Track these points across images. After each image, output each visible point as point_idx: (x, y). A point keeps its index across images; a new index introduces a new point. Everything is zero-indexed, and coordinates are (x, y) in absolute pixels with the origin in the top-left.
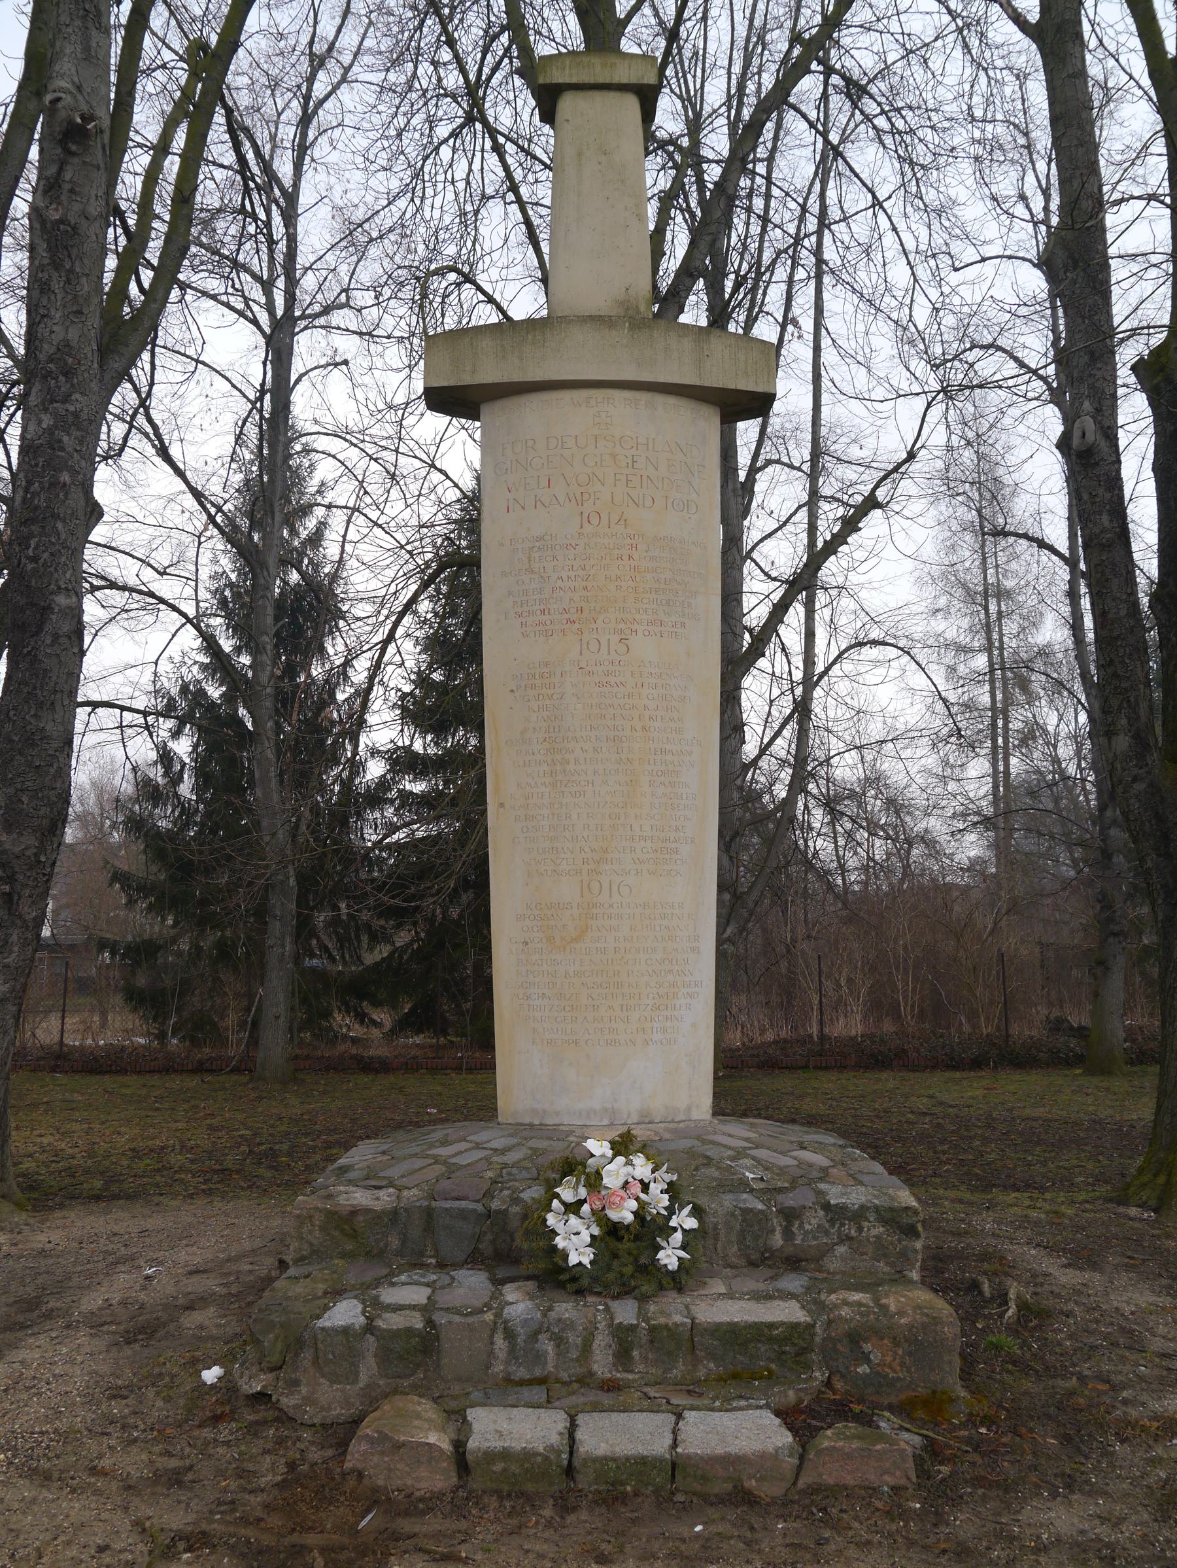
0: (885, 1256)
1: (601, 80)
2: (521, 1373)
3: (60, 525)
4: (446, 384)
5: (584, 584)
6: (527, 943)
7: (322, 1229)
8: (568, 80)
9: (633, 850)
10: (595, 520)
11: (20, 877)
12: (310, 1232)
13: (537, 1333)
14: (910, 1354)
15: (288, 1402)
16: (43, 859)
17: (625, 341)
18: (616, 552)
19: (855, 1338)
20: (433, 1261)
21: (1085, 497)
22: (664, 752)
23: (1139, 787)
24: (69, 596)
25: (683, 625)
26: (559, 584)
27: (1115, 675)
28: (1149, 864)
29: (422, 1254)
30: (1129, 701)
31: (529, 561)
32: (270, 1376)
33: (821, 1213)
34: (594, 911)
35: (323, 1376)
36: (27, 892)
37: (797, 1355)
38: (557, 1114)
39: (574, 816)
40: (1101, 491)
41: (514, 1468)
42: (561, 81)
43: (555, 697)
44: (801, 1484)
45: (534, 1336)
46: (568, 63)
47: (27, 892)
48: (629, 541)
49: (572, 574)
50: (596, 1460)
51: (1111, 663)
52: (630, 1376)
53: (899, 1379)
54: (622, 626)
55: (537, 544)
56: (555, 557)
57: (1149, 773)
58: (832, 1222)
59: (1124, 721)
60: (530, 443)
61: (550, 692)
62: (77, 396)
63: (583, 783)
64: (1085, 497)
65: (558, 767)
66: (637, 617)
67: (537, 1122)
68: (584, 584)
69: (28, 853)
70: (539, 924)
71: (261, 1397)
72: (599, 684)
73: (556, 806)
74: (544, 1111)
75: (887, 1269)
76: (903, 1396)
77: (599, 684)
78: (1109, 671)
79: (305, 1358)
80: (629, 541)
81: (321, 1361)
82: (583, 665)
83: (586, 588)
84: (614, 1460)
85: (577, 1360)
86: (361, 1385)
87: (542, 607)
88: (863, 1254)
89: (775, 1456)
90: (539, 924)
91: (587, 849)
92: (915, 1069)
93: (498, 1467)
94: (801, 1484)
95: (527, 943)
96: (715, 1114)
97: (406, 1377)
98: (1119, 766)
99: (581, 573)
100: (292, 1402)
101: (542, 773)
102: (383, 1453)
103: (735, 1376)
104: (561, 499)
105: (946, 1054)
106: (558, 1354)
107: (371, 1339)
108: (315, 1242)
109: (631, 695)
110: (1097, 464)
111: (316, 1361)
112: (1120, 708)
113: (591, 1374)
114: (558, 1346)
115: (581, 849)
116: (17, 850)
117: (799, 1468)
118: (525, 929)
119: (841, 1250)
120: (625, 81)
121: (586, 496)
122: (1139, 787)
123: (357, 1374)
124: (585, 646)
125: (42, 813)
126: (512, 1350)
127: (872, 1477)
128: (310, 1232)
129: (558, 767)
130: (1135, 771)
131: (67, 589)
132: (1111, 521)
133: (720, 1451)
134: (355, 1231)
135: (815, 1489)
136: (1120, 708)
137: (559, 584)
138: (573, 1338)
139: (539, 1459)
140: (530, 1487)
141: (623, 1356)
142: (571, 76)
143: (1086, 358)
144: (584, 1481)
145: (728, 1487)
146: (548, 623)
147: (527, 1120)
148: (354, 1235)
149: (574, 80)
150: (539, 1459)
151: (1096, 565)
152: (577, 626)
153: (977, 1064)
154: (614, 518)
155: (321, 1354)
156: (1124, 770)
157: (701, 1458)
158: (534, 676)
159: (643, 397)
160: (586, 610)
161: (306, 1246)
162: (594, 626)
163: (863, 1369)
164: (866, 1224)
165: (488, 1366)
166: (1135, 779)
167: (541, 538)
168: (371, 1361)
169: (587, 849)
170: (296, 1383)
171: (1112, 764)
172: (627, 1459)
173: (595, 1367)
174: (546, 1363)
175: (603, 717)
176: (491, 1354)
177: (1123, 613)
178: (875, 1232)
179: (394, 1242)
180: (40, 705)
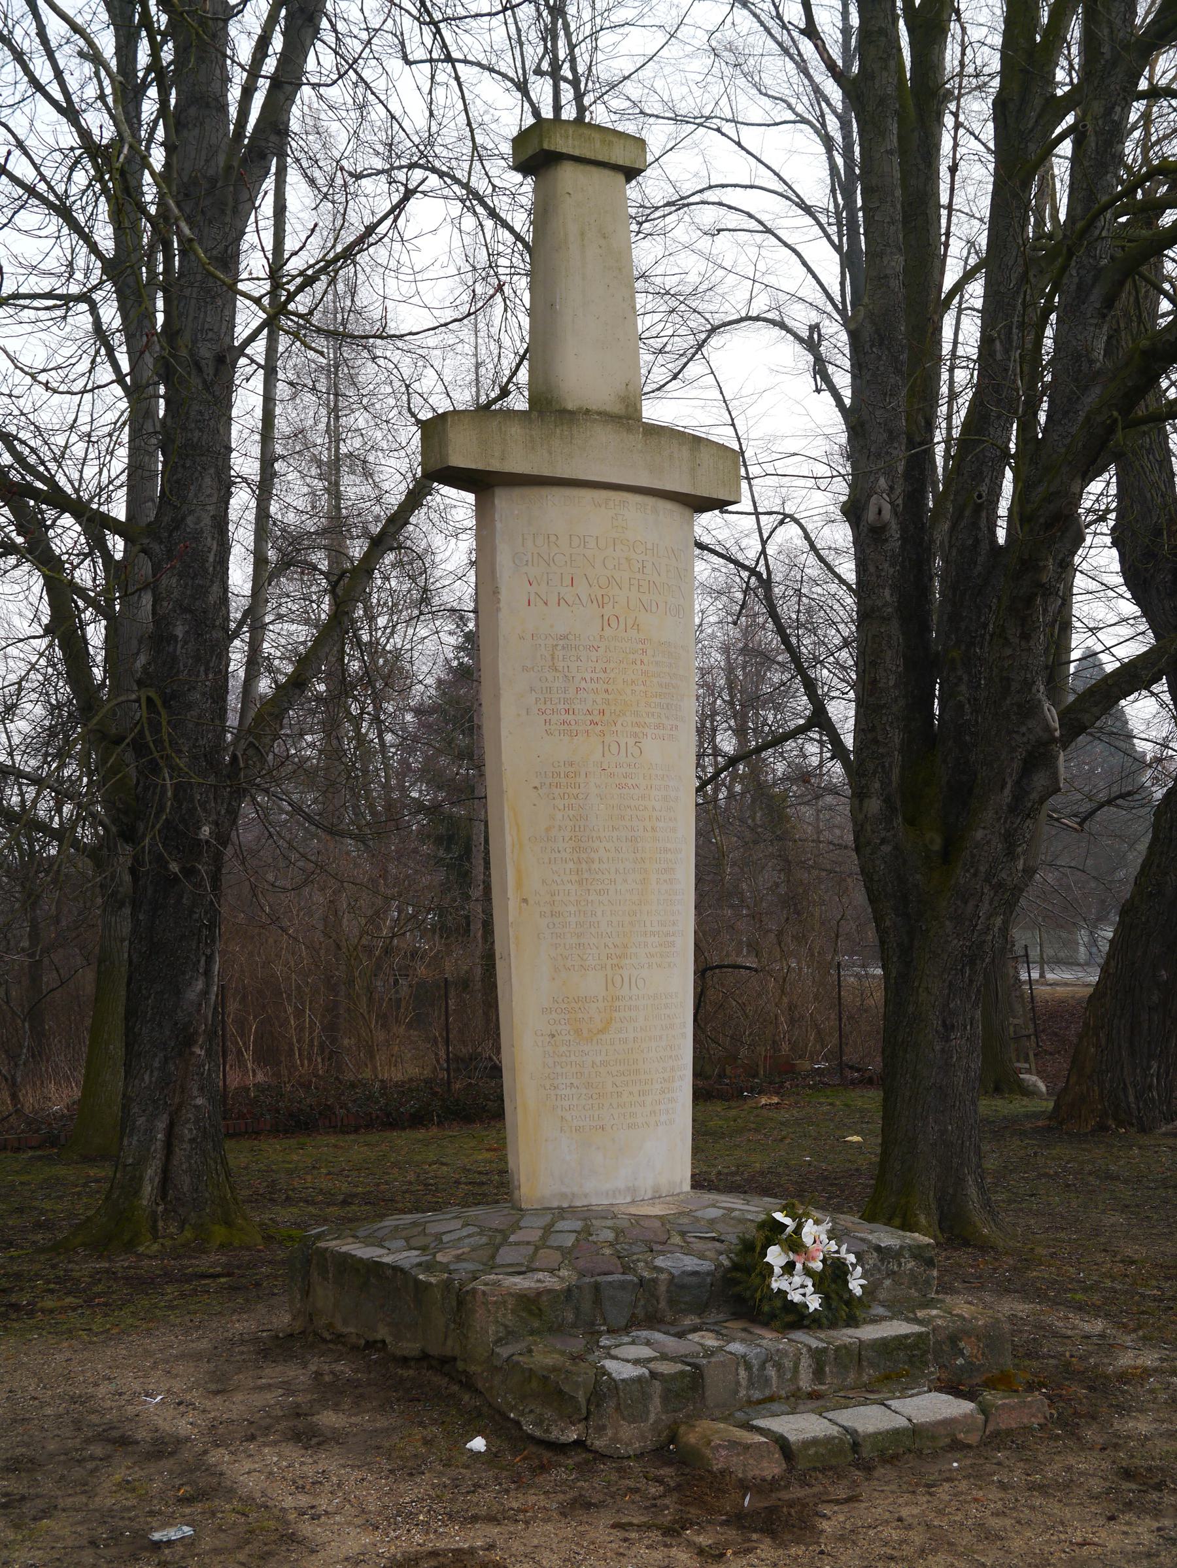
0: (916, 1284)
1: (600, 158)
2: (757, 1395)
4: (473, 467)
5: (605, 686)
6: (553, 1036)
7: (513, 1312)
8: (571, 151)
9: (646, 944)
10: (614, 624)
12: (504, 1315)
13: (764, 1363)
14: (987, 1346)
15: (599, 1443)
17: (639, 446)
18: (631, 656)
19: (953, 1339)
20: (604, 1328)
21: (872, 569)
22: (666, 850)
23: (887, 849)
26: (583, 684)
27: (875, 741)
28: (888, 923)
29: (593, 1324)
30: (883, 766)
31: (553, 658)
32: (581, 1426)
33: (875, 1254)
34: (617, 1003)
35: (624, 1419)
37: (922, 1356)
38: (586, 1196)
39: (599, 913)
40: (886, 565)
41: (822, 1450)
42: (564, 151)
43: (581, 796)
44: (987, 1433)
45: (762, 1367)
46: (571, 132)
48: (640, 646)
49: (595, 676)
50: (870, 1436)
51: (873, 729)
52: (823, 1387)
53: (983, 1365)
54: (637, 729)
55: (561, 642)
56: (578, 658)
57: (894, 836)
58: (882, 1260)
59: (877, 785)
60: (553, 538)
61: (575, 791)
63: (606, 882)
64: (872, 569)
65: (584, 866)
66: (647, 720)
67: (565, 1205)
68: (605, 686)
70: (567, 1017)
71: (579, 1444)
72: (620, 786)
73: (583, 903)
74: (573, 1194)
75: (916, 1294)
76: (984, 1378)
77: (620, 786)
78: (869, 736)
79: (608, 1407)
80: (640, 646)
81: (622, 1407)
82: (605, 766)
83: (607, 691)
84: (880, 1433)
85: (791, 1380)
86: (651, 1421)
87: (567, 706)
88: (902, 1284)
89: (971, 1416)
90: (567, 1017)
91: (611, 945)
92: (344, 1130)
93: (811, 1451)
94: (987, 1433)
95: (553, 1036)
96: (693, 1187)
97: (680, 1410)
98: (869, 828)
99: (602, 675)
100: (603, 1443)
101: (568, 872)
102: (738, 1454)
103: (888, 1378)
104: (584, 599)
105: (380, 1109)
106: (779, 1377)
107: (657, 1383)
108: (509, 1324)
109: (643, 797)
110: (886, 540)
111: (618, 1408)
112: (875, 773)
113: (799, 1389)
114: (778, 1371)
115: (606, 946)
117: (986, 1422)
118: (552, 1022)
119: (888, 1282)
120: (621, 162)
121: (606, 599)
122: (887, 849)
123: (648, 1412)
124: (606, 748)
127: (1025, 1421)
128: (504, 1315)
129: (584, 866)
130: (883, 834)
132: (892, 595)
133: (939, 1418)
134: (540, 1310)
135: (997, 1434)
136: (875, 773)
137: (583, 684)
138: (788, 1364)
139: (837, 1441)
140: (833, 1462)
141: (818, 1374)
142: (574, 147)
143: (885, 436)
144: (866, 1452)
145: (948, 1440)
146: (573, 722)
147: (555, 1205)
148: (540, 1314)
149: (577, 153)
150: (837, 1441)
151: (874, 636)
152: (599, 728)
153: (418, 1120)
154: (630, 622)
155: (622, 1401)
156: (873, 832)
157: (930, 1423)
158: (559, 774)
159: (650, 501)
160: (607, 713)
161: (501, 1329)
162: (614, 729)
163: (960, 1361)
164: (903, 1260)
165: (736, 1392)
166: (883, 841)
167: (565, 637)
168: (657, 1401)
169: (611, 945)
170: (603, 1428)
171: (862, 826)
172: (887, 1432)
173: (801, 1383)
174: (771, 1385)
175: (623, 818)
176: (738, 1383)
177: (891, 683)
178: (909, 1266)
179: (570, 1317)
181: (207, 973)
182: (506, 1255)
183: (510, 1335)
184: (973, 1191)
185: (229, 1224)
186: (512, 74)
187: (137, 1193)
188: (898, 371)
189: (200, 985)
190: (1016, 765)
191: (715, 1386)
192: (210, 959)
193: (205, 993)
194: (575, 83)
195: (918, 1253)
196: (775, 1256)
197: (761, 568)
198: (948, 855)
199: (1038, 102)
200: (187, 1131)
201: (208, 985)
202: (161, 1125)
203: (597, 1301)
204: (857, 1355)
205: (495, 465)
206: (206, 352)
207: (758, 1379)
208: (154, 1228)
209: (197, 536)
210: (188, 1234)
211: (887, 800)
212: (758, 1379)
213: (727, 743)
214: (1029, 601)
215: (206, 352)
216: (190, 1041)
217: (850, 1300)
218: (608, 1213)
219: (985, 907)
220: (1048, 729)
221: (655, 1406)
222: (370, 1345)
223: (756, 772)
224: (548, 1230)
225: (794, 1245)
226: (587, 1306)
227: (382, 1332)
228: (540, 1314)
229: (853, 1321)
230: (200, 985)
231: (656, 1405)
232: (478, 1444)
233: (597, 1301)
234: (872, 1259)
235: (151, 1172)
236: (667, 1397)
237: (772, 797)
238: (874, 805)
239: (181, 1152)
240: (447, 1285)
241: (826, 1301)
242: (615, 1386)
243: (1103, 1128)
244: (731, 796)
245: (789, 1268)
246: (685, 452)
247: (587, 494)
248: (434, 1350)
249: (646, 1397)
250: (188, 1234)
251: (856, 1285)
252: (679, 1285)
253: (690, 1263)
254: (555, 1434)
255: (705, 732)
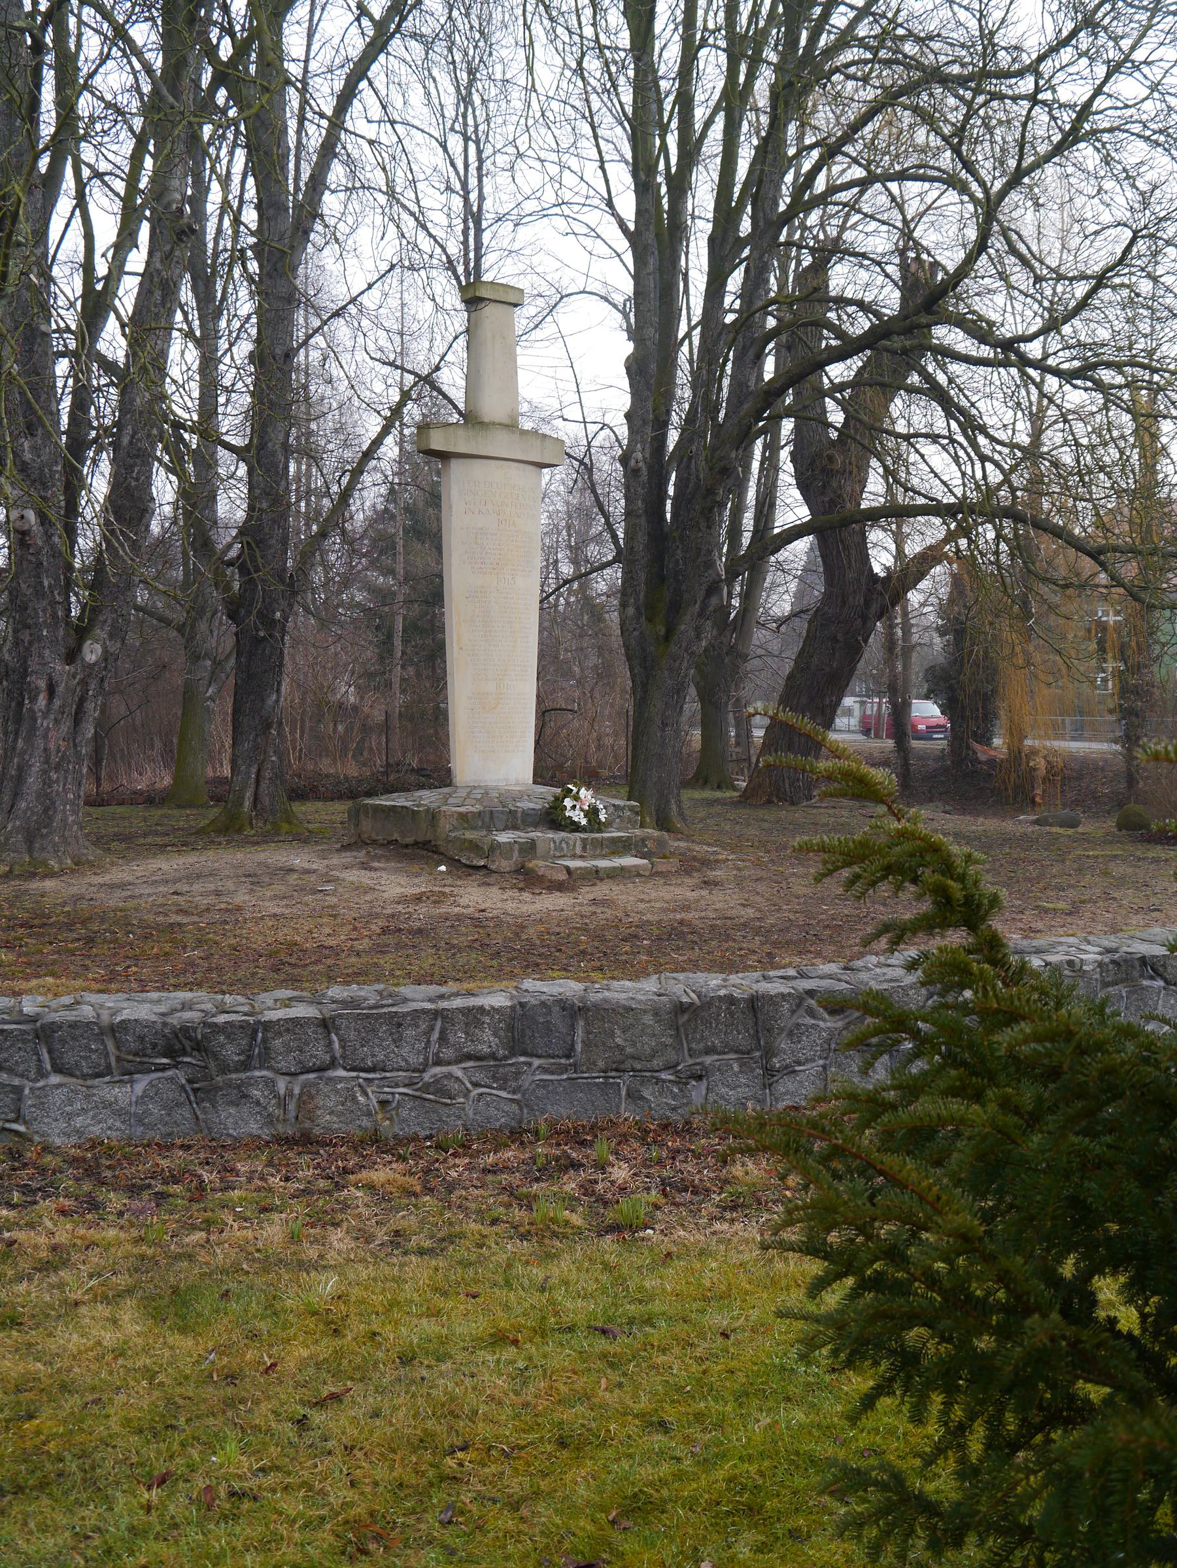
15: (493, 867)
23: (636, 633)
71: (484, 867)
92: (326, 799)
122: (636, 633)
141: (584, 848)
148: (467, 821)
181: (278, 691)
182: (451, 801)
183: (455, 829)
184: (674, 807)
185: (289, 823)
186: (437, 135)
187: (241, 804)
188: (649, 389)
189: (274, 697)
190: (703, 593)
191: (541, 848)
192: (279, 684)
193: (277, 701)
194: (477, 142)
195: (631, 809)
196: (568, 802)
197: (587, 460)
198: (667, 638)
199: (731, 240)
200: (267, 774)
201: (279, 697)
202: (254, 770)
203: (491, 818)
204: (601, 843)
205: (451, 449)
206: (279, 351)
207: (558, 848)
208: (251, 824)
209: (273, 453)
210: (268, 827)
211: (637, 609)
212: (558, 848)
213: (566, 569)
214: (711, 510)
215: (279, 351)
216: (269, 726)
217: (600, 822)
218: (495, 788)
219: (685, 664)
220: (719, 575)
221: (516, 854)
222: (390, 843)
223: (583, 588)
224: (469, 793)
225: (576, 798)
226: (487, 819)
227: (396, 836)
228: (467, 821)
229: (599, 831)
230: (274, 697)
231: (516, 854)
232: (443, 868)
233: (491, 818)
234: (611, 809)
235: (249, 794)
236: (520, 851)
237: (594, 606)
238: (631, 611)
239: (264, 784)
240: (428, 811)
241: (589, 821)
242: (499, 844)
243: (769, 802)
244: (568, 603)
245: (574, 807)
246: (539, 442)
247: (493, 462)
248: (420, 839)
249: (512, 850)
250: (268, 827)
251: (603, 817)
252: (526, 814)
253: (532, 805)
254: (475, 863)
255: (549, 552)
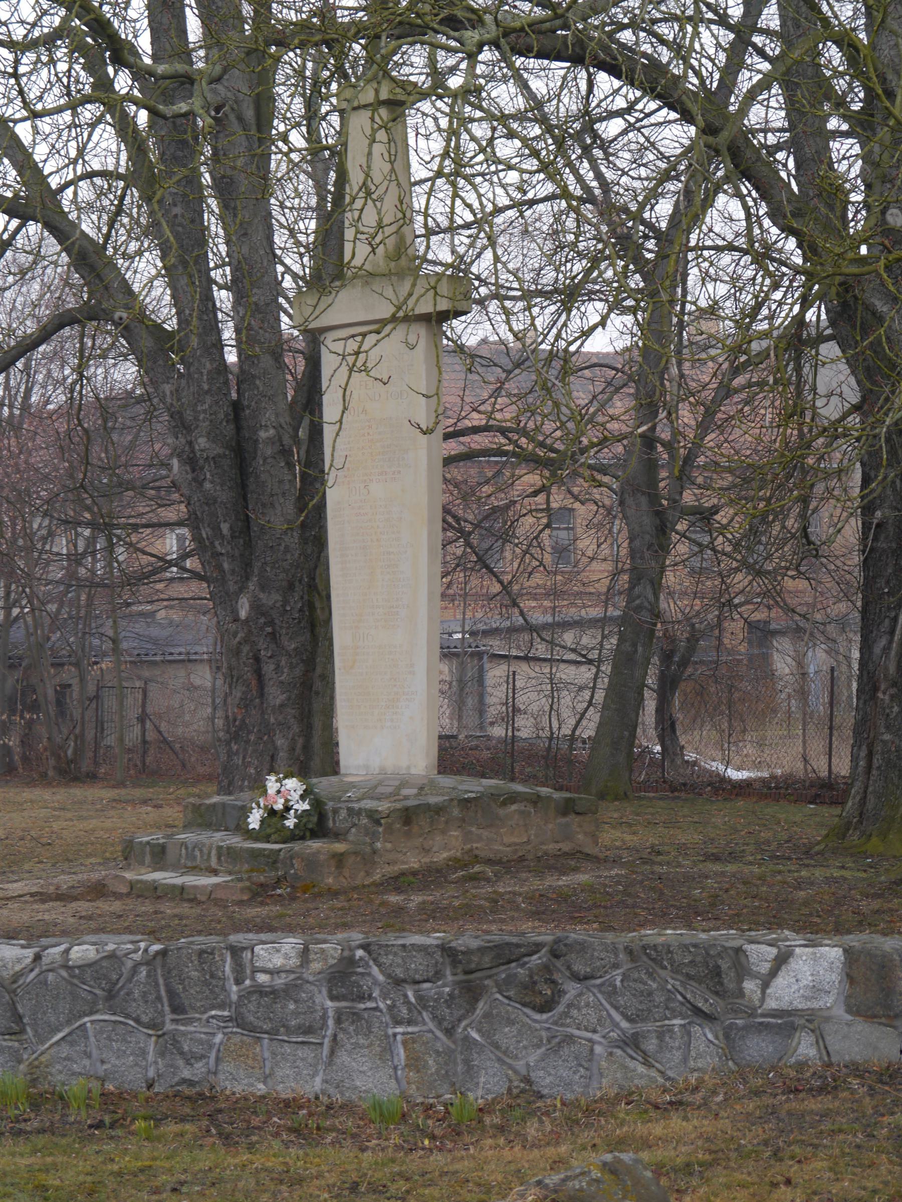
3: (258, 382)
11: (277, 621)
16: (288, 608)
24: (267, 431)
25: (399, 472)
36: (284, 631)
47: (284, 631)
62: (255, 291)
69: (278, 605)
96: (439, 773)
116: (270, 603)
125: (280, 577)
126: (187, 854)
131: (266, 426)
138: (205, 851)
165: (179, 860)
180: (264, 505)
